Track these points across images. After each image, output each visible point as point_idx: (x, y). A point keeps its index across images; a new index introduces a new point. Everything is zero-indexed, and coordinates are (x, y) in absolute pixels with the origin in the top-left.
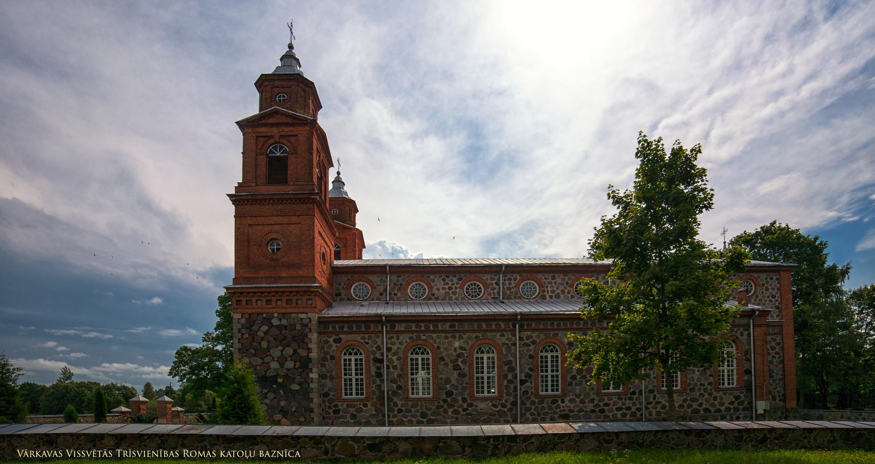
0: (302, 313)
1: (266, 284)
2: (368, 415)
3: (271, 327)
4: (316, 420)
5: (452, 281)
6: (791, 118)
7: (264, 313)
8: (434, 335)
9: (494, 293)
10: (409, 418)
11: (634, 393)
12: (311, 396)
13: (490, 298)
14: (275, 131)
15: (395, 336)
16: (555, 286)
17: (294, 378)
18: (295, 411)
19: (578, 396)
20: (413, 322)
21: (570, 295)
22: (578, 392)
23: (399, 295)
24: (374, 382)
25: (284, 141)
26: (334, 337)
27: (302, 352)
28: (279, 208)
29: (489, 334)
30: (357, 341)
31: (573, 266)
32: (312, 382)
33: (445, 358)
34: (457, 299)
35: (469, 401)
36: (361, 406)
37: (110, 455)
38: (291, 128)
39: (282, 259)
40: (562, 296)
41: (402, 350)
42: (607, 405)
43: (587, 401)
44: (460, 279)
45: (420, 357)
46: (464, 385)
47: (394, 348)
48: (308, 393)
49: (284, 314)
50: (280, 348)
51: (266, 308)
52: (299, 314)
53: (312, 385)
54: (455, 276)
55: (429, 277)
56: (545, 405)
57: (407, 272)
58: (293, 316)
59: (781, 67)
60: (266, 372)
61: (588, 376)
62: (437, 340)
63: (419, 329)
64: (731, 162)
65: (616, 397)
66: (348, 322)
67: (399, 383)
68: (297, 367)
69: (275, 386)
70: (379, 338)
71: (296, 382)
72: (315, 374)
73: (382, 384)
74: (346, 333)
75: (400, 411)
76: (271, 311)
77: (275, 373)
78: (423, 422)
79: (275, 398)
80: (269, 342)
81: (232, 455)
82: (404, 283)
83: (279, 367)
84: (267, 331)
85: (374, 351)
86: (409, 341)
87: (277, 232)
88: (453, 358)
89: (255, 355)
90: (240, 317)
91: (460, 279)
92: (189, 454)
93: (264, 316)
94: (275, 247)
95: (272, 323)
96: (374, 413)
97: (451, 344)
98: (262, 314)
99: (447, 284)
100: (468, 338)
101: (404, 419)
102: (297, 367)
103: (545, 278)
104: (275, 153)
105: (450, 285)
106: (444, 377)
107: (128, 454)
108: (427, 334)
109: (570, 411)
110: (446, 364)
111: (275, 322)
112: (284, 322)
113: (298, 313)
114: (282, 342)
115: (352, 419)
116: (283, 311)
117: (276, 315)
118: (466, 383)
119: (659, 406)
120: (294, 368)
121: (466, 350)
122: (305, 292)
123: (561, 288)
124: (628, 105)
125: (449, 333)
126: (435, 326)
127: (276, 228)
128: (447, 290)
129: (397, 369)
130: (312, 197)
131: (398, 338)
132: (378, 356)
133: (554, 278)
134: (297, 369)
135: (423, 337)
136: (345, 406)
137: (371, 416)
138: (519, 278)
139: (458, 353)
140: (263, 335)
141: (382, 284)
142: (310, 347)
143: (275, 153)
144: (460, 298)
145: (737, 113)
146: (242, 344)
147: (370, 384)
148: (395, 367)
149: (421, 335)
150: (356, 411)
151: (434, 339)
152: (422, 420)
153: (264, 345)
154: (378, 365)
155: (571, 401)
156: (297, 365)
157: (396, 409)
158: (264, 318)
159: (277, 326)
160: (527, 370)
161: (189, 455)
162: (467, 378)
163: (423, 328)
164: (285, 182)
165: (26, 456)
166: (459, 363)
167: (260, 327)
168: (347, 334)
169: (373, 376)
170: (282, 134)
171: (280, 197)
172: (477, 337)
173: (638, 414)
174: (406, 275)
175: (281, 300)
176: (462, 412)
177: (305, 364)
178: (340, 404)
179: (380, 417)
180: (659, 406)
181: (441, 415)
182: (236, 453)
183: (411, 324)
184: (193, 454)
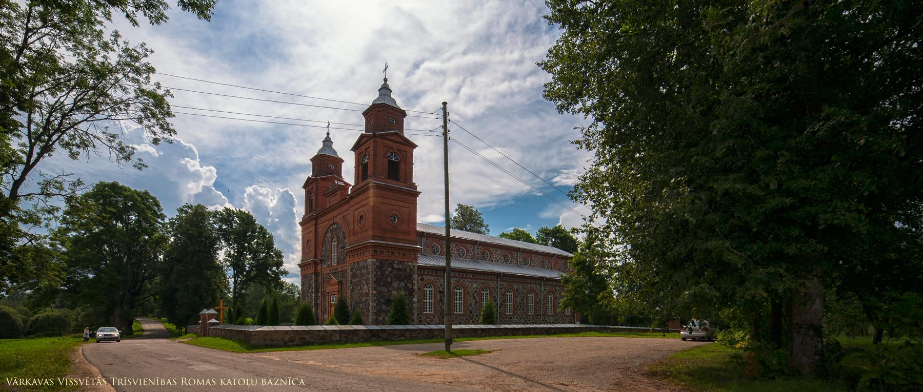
6: (519, 100)
11: (538, 316)
12: (414, 312)
23: (427, 250)
26: (420, 277)
29: (487, 281)
37: (104, 383)
49: (400, 261)
50: (398, 282)
54: (454, 243)
56: (507, 319)
59: (516, 55)
64: (474, 120)
66: (428, 269)
74: (427, 275)
80: (392, 278)
82: (430, 243)
87: (396, 210)
89: (383, 286)
91: (456, 245)
92: (187, 382)
93: (390, 261)
96: (438, 322)
97: (472, 285)
100: (480, 283)
106: (469, 303)
107: (123, 382)
110: (470, 296)
111: (396, 266)
112: (401, 266)
114: (399, 278)
116: (400, 260)
117: (396, 262)
123: (499, 257)
124: (397, 35)
127: (396, 208)
133: (496, 251)
136: (424, 318)
140: (389, 273)
145: (482, 79)
146: (377, 278)
155: (517, 318)
156: (407, 293)
160: (501, 301)
161: (188, 384)
174: (431, 239)
177: (411, 292)
178: (422, 316)
182: (237, 381)
184: (192, 382)
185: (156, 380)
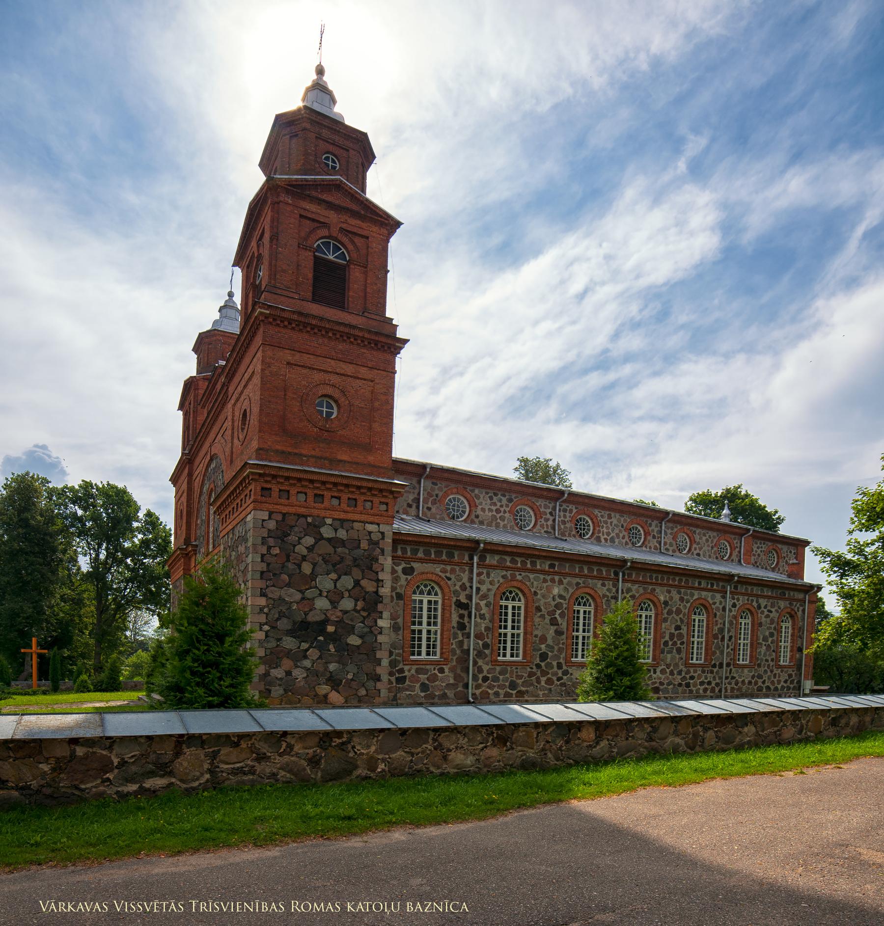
0: (371, 523)
1: (314, 467)
2: (444, 684)
3: (320, 540)
4: (384, 693)
5: (500, 501)
7: (310, 516)
8: (532, 576)
9: (547, 525)
10: (496, 689)
11: (714, 666)
13: (542, 531)
14: (332, 217)
15: (485, 571)
16: (611, 528)
17: (353, 627)
18: (352, 680)
19: (668, 666)
20: (509, 555)
21: (624, 541)
22: (668, 661)
23: (434, 510)
24: (455, 636)
25: (345, 240)
26: (403, 565)
27: (368, 585)
28: (340, 347)
29: (590, 581)
30: (437, 575)
31: (630, 505)
32: (381, 633)
33: (542, 608)
34: (505, 526)
35: (565, 668)
36: (436, 672)
38: (358, 222)
39: (340, 432)
40: (617, 540)
41: (493, 592)
42: (692, 678)
43: (675, 672)
44: (510, 500)
45: (510, 604)
46: (561, 646)
47: (484, 588)
48: (374, 651)
49: (342, 521)
50: (334, 576)
51: (314, 508)
52: (367, 525)
53: (381, 638)
54: (504, 496)
55: (473, 491)
57: (447, 479)
58: (356, 525)
60: (306, 614)
61: (679, 642)
62: (535, 583)
63: (514, 566)
65: (701, 669)
67: (486, 640)
68: (358, 608)
69: (321, 638)
70: (464, 572)
71: (356, 632)
72: (385, 621)
73: (466, 640)
74: (421, 560)
75: (485, 679)
76: (322, 513)
77: (323, 617)
78: (512, 694)
79: (320, 657)
80: (315, 565)
81: (365, 909)
83: (330, 607)
84: (313, 546)
85: (457, 591)
86: (502, 580)
87: (333, 386)
88: (551, 609)
89: (289, 585)
90: (267, 518)
91: (510, 500)
93: (310, 520)
94: (325, 410)
95: (321, 534)
96: (452, 681)
97: (549, 589)
98: (306, 517)
99: (495, 504)
100: (569, 584)
101: (490, 691)
102: (358, 608)
103: (602, 516)
104: (326, 254)
105: (498, 507)
106: (539, 633)
107: (208, 907)
108: (523, 574)
109: (662, 684)
110: (543, 616)
111: (327, 532)
112: (342, 534)
113: (364, 522)
114: (336, 566)
115: (422, 691)
116: (342, 516)
118: (563, 644)
119: (733, 681)
120: (355, 610)
121: (565, 600)
122: (381, 491)
125: (549, 575)
126: (533, 564)
127: (334, 379)
128: (494, 513)
129: (485, 619)
130: (397, 344)
131: (488, 575)
132: (464, 600)
133: (610, 517)
134: (358, 612)
135: (519, 578)
136: (413, 672)
137: (448, 686)
138: (575, 511)
139: (556, 602)
140: (305, 552)
141: (412, 491)
142: (380, 578)
143: (326, 254)
144: (509, 526)
146: (268, 564)
147: (450, 640)
148: (482, 617)
149: (517, 573)
150: (428, 679)
151: (532, 580)
152: (511, 691)
153: (307, 568)
154: (462, 612)
156: (360, 605)
157: (481, 676)
158: (309, 524)
159: (329, 540)
161: (300, 909)
162: (564, 636)
163: (519, 565)
164: (341, 304)
165: (52, 910)
166: (557, 616)
167: (300, 538)
168: (422, 563)
169: (453, 627)
170: (344, 226)
171: (347, 330)
172: (578, 584)
173: (717, 690)
174: (444, 484)
175: (339, 498)
176: (556, 682)
178: (406, 668)
179: (460, 689)
180: (733, 681)
181: (532, 684)
183: (506, 557)
185: (255, 904)
